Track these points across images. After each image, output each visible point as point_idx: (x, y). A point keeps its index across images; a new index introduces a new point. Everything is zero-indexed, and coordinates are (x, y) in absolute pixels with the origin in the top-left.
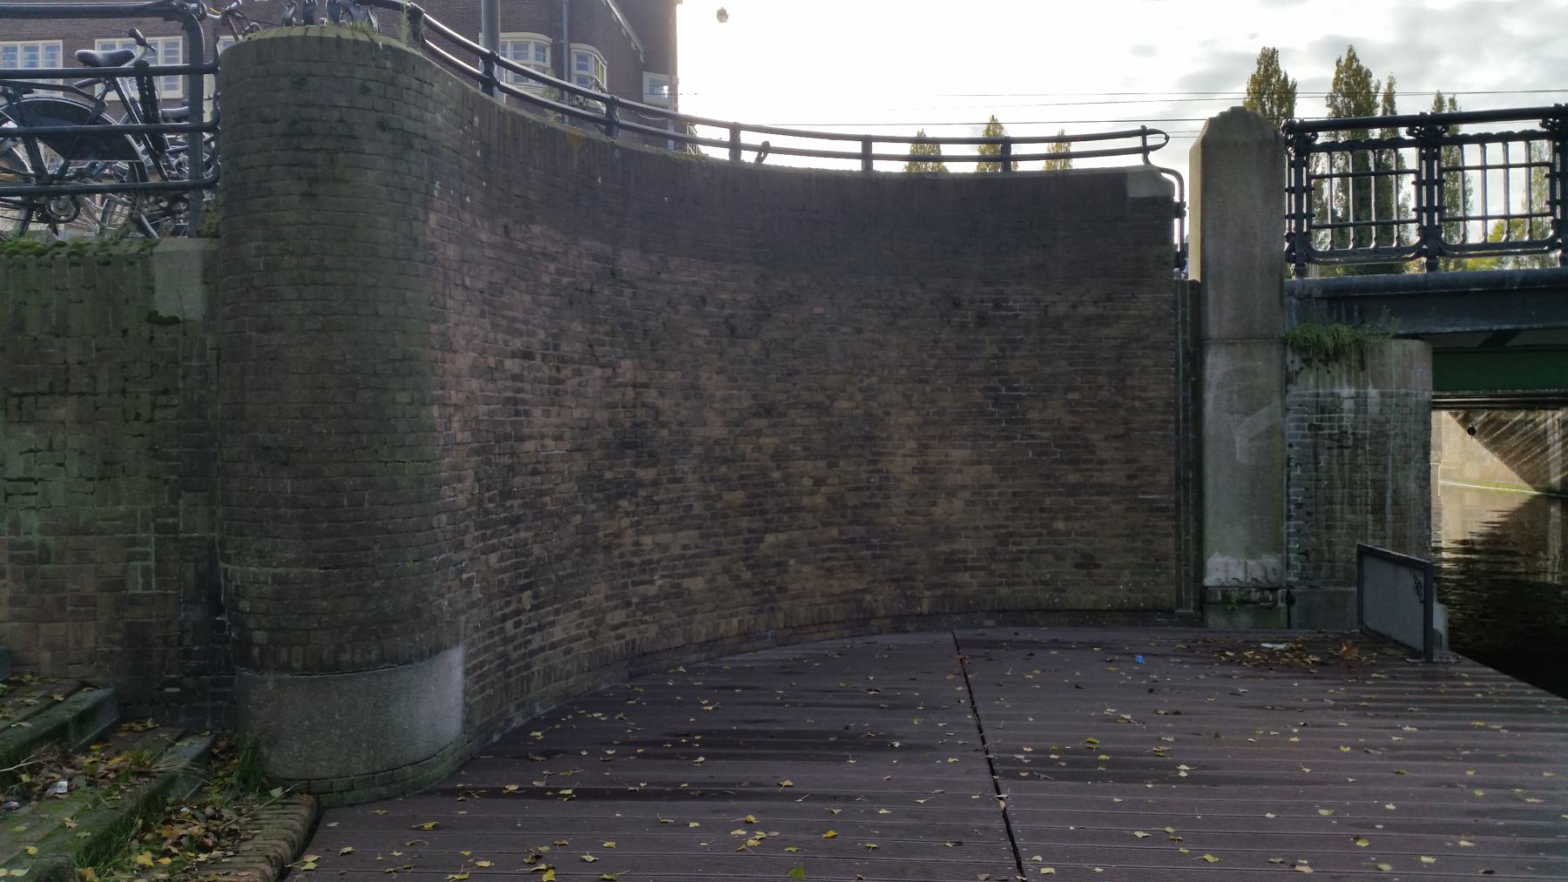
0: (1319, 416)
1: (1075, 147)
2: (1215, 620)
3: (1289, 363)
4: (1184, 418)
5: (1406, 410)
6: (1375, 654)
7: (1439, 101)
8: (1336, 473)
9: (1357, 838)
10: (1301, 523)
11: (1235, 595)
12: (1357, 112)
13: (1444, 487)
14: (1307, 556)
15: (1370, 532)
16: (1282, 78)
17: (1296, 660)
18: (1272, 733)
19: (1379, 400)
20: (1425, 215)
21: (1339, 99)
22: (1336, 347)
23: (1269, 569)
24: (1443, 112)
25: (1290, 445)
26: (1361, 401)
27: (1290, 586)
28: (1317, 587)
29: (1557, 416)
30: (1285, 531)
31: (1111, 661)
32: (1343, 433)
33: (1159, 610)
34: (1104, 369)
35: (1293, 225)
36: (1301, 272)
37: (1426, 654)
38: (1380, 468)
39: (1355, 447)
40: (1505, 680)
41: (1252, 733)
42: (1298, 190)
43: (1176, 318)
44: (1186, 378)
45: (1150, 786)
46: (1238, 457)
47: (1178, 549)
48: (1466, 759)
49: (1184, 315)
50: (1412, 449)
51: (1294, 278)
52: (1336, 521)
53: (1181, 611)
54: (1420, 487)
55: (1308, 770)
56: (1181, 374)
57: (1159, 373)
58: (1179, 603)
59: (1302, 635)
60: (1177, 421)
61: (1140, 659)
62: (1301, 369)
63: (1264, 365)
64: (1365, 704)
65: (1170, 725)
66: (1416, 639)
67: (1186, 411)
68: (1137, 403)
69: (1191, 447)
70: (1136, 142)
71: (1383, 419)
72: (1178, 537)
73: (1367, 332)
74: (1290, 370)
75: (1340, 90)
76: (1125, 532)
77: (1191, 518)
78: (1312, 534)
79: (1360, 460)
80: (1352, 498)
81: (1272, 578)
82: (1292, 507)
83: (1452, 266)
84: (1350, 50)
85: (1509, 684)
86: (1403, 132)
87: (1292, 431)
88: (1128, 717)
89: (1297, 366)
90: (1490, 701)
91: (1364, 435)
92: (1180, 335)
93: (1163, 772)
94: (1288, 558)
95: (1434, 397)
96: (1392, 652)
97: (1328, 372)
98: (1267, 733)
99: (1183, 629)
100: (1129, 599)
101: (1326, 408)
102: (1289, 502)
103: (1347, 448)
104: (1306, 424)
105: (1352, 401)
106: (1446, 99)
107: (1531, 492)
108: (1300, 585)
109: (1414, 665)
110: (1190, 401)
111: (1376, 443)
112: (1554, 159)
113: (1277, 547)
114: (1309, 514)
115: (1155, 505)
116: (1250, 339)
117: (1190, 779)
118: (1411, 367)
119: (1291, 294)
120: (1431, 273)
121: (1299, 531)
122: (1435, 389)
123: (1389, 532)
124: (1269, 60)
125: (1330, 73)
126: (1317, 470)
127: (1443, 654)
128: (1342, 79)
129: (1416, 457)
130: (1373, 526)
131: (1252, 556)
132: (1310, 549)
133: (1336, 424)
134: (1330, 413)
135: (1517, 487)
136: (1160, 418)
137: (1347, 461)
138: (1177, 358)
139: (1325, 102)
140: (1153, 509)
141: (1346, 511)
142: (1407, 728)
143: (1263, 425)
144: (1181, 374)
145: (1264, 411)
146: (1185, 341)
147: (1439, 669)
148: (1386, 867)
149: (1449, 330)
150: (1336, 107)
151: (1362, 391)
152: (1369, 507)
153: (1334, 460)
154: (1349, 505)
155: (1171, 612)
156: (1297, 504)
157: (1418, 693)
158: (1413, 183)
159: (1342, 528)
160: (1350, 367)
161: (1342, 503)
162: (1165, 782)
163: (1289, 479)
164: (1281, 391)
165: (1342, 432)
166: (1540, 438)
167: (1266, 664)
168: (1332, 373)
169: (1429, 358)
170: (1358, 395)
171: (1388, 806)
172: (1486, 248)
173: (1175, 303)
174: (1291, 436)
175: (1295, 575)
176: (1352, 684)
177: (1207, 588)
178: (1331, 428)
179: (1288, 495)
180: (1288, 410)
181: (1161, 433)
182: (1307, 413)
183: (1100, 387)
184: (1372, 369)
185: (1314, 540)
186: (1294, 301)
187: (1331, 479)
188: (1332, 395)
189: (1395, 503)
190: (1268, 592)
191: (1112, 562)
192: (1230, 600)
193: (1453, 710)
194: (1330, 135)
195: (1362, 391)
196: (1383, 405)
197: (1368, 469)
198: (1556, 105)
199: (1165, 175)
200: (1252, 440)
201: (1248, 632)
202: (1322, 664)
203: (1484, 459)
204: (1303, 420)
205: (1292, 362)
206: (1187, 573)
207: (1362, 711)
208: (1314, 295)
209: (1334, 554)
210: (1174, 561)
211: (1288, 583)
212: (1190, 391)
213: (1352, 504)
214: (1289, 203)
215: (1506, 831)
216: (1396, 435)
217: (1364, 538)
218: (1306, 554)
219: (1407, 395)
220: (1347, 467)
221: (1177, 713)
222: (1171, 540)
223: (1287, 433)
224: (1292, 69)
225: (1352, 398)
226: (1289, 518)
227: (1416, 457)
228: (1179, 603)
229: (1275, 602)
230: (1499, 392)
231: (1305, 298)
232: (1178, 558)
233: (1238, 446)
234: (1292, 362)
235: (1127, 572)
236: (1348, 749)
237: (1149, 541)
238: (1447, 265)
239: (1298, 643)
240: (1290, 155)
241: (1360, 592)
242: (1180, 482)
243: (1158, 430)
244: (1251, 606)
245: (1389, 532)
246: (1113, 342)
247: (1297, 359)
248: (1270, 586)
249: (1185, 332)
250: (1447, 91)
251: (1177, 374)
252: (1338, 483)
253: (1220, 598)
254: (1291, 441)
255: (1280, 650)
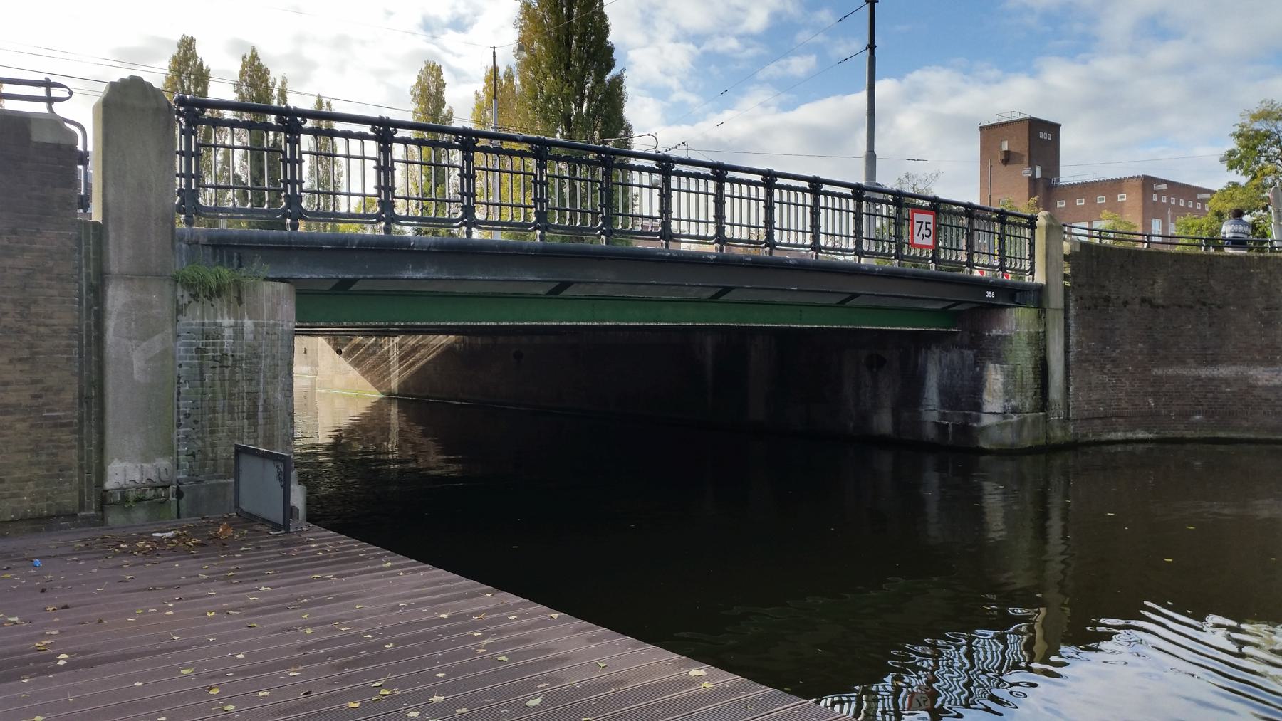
0: (205, 341)
1: (339, 126)
2: (114, 518)
3: (179, 297)
4: (87, 343)
5: (274, 337)
6: (246, 531)
7: (320, 102)
8: (218, 388)
9: (210, 689)
10: (188, 429)
11: (132, 495)
12: (259, 98)
13: (320, 394)
14: (194, 457)
15: (245, 434)
16: (198, 62)
17: (181, 544)
18: (150, 611)
19: (253, 328)
20: (604, 209)
21: (244, 88)
22: (218, 286)
23: (162, 470)
24: (322, 110)
25: (180, 366)
26: (238, 330)
27: (179, 482)
28: (202, 482)
29: (395, 342)
30: (176, 438)
31: (8, 569)
32: (224, 355)
33: (63, 515)
34: (9, 297)
35: (183, 183)
36: (189, 222)
37: (285, 527)
38: (254, 383)
39: (234, 366)
40: (340, 539)
41: (133, 614)
42: (187, 154)
43: (80, 253)
44: (89, 308)
45: (25, 681)
46: (136, 377)
47: (81, 459)
48: (304, 605)
49: (87, 252)
50: (279, 368)
51: (184, 226)
52: (218, 427)
53: (83, 514)
54: (285, 396)
55: (176, 638)
56: (84, 304)
57: (64, 302)
58: (82, 507)
59: (187, 522)
60: (81, 346)
61: (37, 562)
62: (190, 302)
63: (159, 298)
64: (232, 573)
65: (57, 619)
66: (277, 515)
67: (88, 336)
68: (42, 329)
69: (93, 368)
70: (41, 92)
71: (256, 344)
72: (81, 446)
73: (243, 275)
74: (180, 303)
75: (245, 80)
76: (31, 447)
77: (93, 431)
78: (198, 438)
79: (238, 377)
80: (231, 407)
81: (165, 477)
82: (182, 417)
83: (329, 228)
84: (253, 50)
85: (343, 541)
86: (272, 119)
87: (182, 354)
88: (16, 619)
89: (186, 300)
90: (328, 557)
91: (241, 357)
92: (84, 269)
93: (41, 665)
94: (178, 459)
95: (296, 327)
96: (259, 528)
97: (212, 305)
98: (146, 611)
99: (85, 529)
100: (33, 508)
101: (211, 335)
102: (179, 413)
103: (227, 367)
104: (194, 348)
105: (231, 329)
106: (325, 101)
107: (378, 395)
108: (187, 480)
109: (275, 536)
110: (93, 328)
111: (251, 363)
112: (463, 164)
113: (169, 451)
114: (196, 422)
115: (59, 421)
116: (147, 275)
117: (70, 666)
118: (278, 304)
119: (181, 240)
120: (294, 232)
121: (187, 436)
122: (298, 320)
123: (261, 433)
124: (187, 46)
125: (236, 67)
126: (202, 385)
127: (299, 523)
128: (247, 72)
129: (282, 373)
130: (249, 429)
131: (147, 460)
132: (196, 451)
133: (218, 348)
134: (213, 339)
135: (370, 393)
136: (65, 342)
137: (227, 378)
138: (80, 289)
139: (232, 88)
140: (58, 425)
141: (226, 418)
142: (263, 589)
143: (158, 349)
144: (84, 304)
145: (157, 337)
146: (88, 275)
147: (294, 537)
148: (230, 708)
149: (307, 276)
150: (242, 94)
151: (239, 321)
152: (245, 414)
153: (217, 377)
154: (229, 413)
155: (74, 515)
156: (186, 414)
157: (275, 558)
158: (375, 168)
159: (223, 432)
160: (230, 302)
161: (223, 412)
162: (44, 674)
163: (179, 393)
164: (173, 320)
165: (223, 355)
166: (385, 359)
167: (155, 550)
168: (215, 306)
169: (293, 296)
170: (236, 325)
171: (238, 656)
172: (351, 217)
173: (79, 239)
174: (181, 358)
175: (184, 474)
176: (223, 559)
177: (107, 491)
178: (214, 351)
179: (178, 407)
180: (178, 336)
181: (65, 356)
182: (194, 339)
183: (5, 314)
184: (247, 304)
185: (199, 443)
186: (184, 246)
187: (214, 392)
188: (216, 324)
189: (265, 410)
190: (160, 489)
191: (16, 476)
192: (127, 500)
193: (300, 568)
194: (237, 115)
195: (239, 321)
196: (256, 333)
197: (244, 384)
198: (380, 116)
199: (67, 125)
200: (147, 361)
201: (143, 525)
202: (203, 545)
203: (348, 373)
204: (191, 345)
205: (182, 296)
206: (89, 480)
207: (229, 580)
208: (200, 243)
209: (216, 453)
210: (77, 470)
211: (178, 481)
212: (93, 318)
213: (231, 412)
214: (180, 164)
215: (325, 657)
216: (266, 357)
217: (241, 439)
218: (193, 455)
219: (275, 325)
220: (227, 383)
221: (66, 607)
222: (75, 451)
223: (178, 355)
224: (206, 54)
225: (231, 327)
226: (179, 426)
227: (282, 373)
228: (82, 507)
229: (167, 498)
230: (345, 324)
231: (193, 244)
232: (81, 468)
233: (135, 367)
234: (182, 296)
235: (30, 484)
236: (213, 614)
237: (52, 454)
238: (325, 227)
239: (185, 529)
240: (181, 124)
241: (237, 483)
242: (83, 399)
243: (62, 354)
244: (146, 502)
245: (261, 433)
246: (17, 272)
247: (186, 294)
248: (163, 484)
249: (88, 267)
250: (326, 93)
251: (80, 304)
252: (220, 396)
253: (119, 499)
254: (181, 362)
255: (167, 538)
